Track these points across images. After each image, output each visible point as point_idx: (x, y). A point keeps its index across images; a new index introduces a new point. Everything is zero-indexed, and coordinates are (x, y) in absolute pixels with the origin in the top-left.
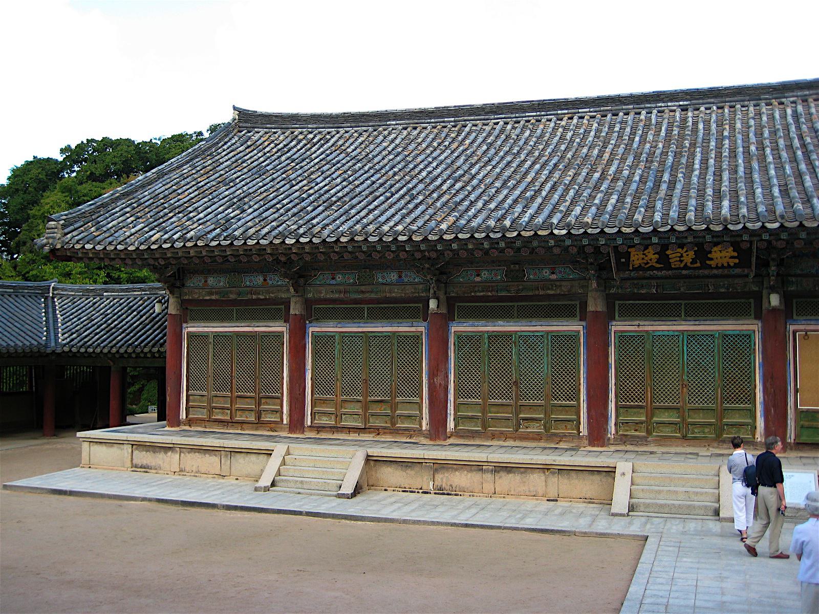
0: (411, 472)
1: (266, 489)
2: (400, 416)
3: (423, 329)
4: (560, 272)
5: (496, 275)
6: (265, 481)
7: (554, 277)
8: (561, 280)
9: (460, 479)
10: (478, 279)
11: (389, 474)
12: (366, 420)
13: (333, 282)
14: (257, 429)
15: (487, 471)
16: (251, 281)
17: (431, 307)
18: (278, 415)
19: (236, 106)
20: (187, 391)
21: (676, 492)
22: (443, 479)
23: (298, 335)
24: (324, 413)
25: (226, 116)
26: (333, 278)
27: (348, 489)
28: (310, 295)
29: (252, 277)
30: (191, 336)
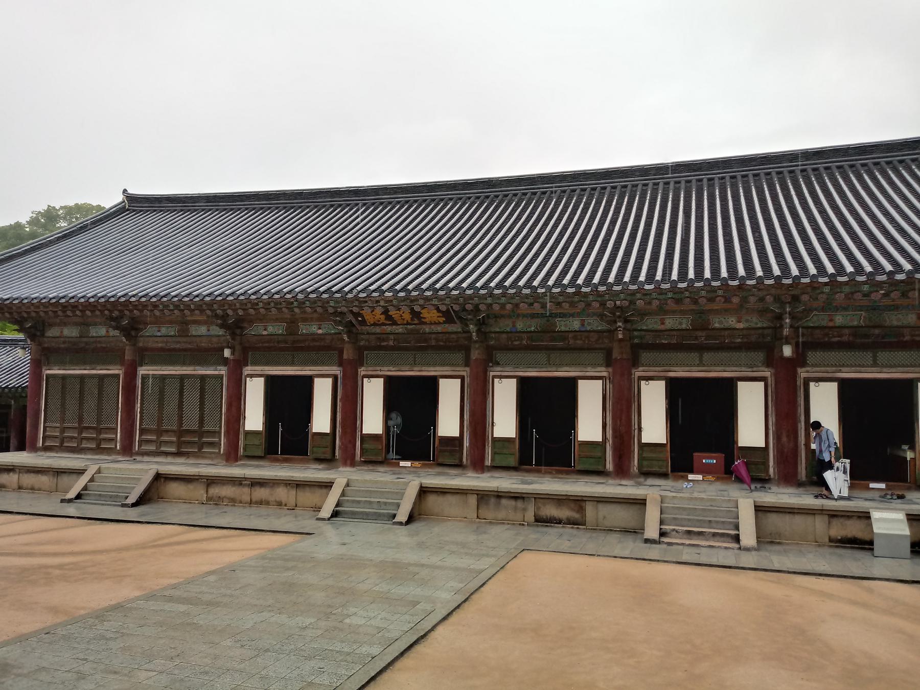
0: (191, 486)
1: (70, 501)
2: (184, 442)
3: (223, 372)
4: (747, 321)
5: (279, 329)
6: (72, 494)
7: (320, 331)
8: (326, 334)
9: (227, 491)
10: (265, 333)
11: (175, 489)
12: (179, 447)
13: (159, 334)
14: (97, 454)
15: (245, 485)
16: (97, 332)
17: (614, 357)
18: (114, 443)
19: (130, 191)
20: (45, 422)
21: (370, 502)
22: (215, 491)
23: (131, 375)
24: (166, 442)
25: (111, 199)
26: (831, 320)
27: (132, 499)
28: (141, 345)
29: (900, 316)
30: (48, 376)
